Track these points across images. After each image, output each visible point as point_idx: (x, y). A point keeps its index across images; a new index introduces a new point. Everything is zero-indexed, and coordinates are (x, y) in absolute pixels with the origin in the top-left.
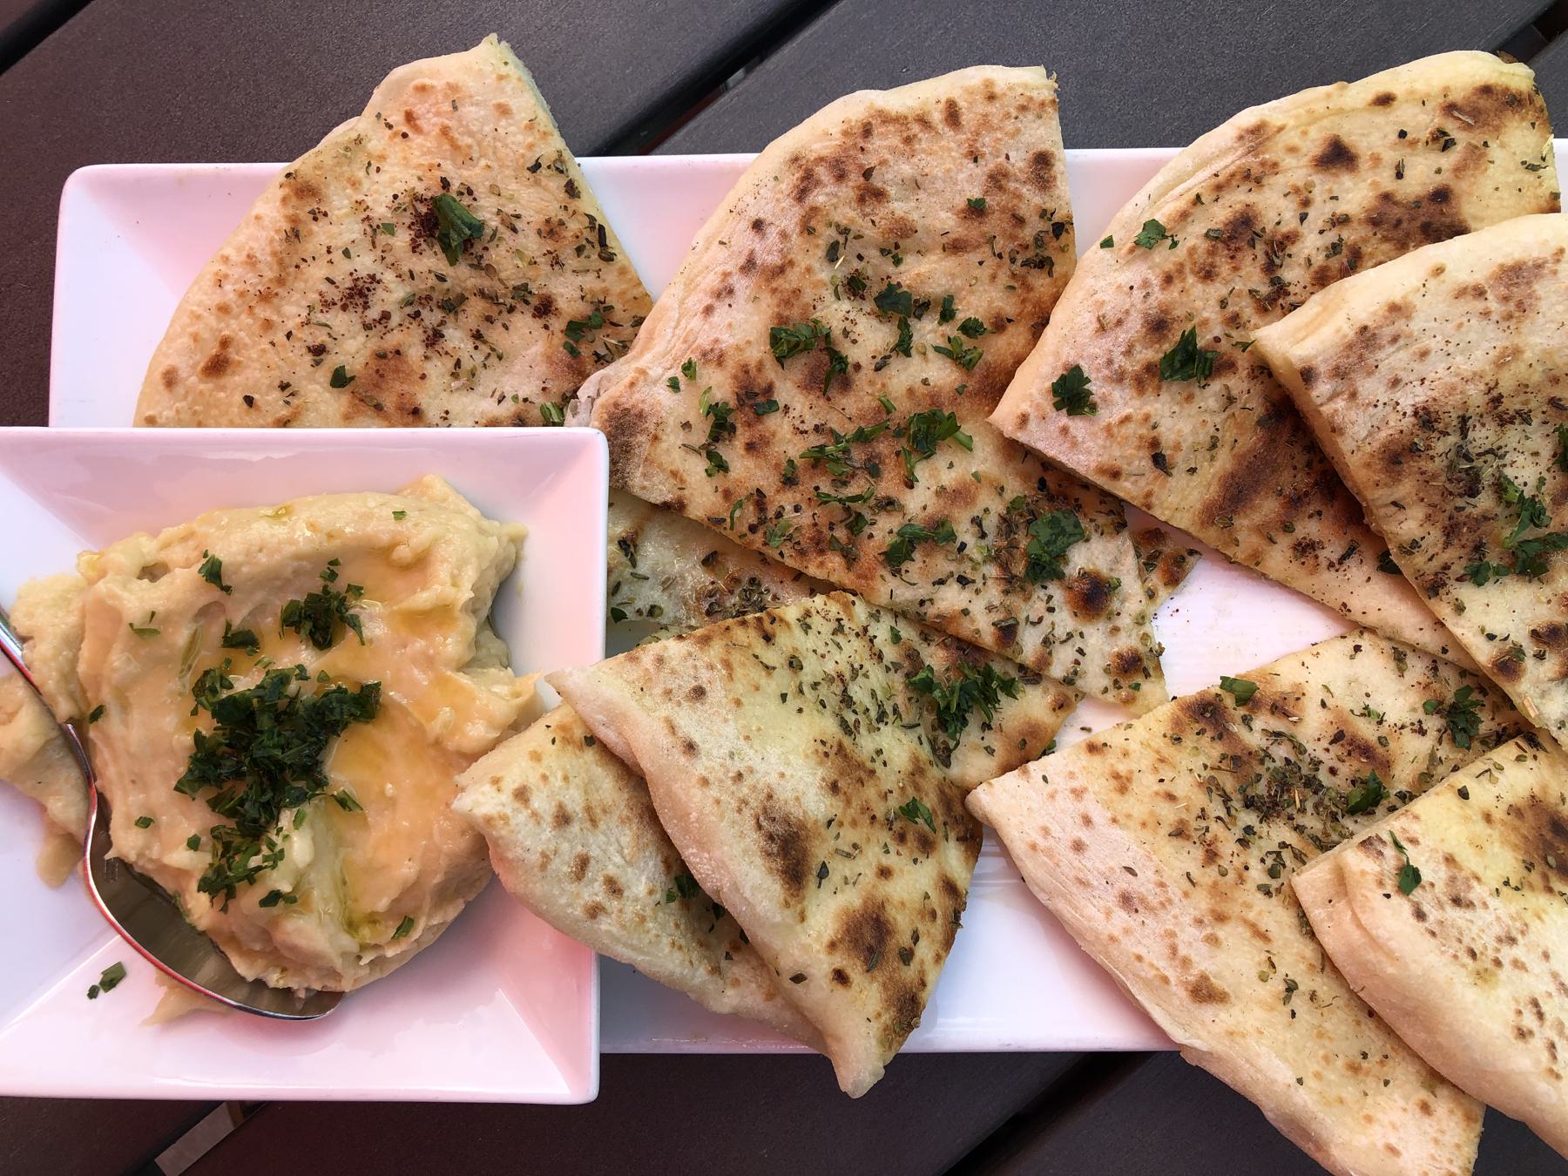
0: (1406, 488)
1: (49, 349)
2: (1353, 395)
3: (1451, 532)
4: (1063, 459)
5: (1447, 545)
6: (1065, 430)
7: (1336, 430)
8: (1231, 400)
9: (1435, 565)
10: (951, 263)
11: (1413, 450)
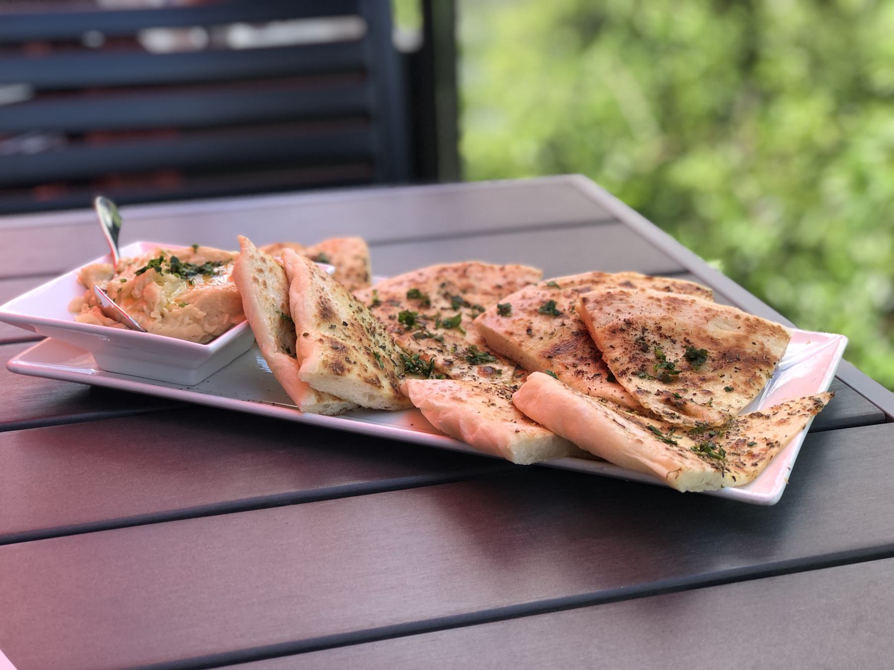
0: (617, 342)
1: (9, 655)
2: (601, 309)
3: (632, 359)
4: (494, 329)
5: (630, 362)
6: (498, 320)
7: (593, 319)
8: (563, 325)
9: (624, 368)
10: (484, 297)
11: (622, 330)
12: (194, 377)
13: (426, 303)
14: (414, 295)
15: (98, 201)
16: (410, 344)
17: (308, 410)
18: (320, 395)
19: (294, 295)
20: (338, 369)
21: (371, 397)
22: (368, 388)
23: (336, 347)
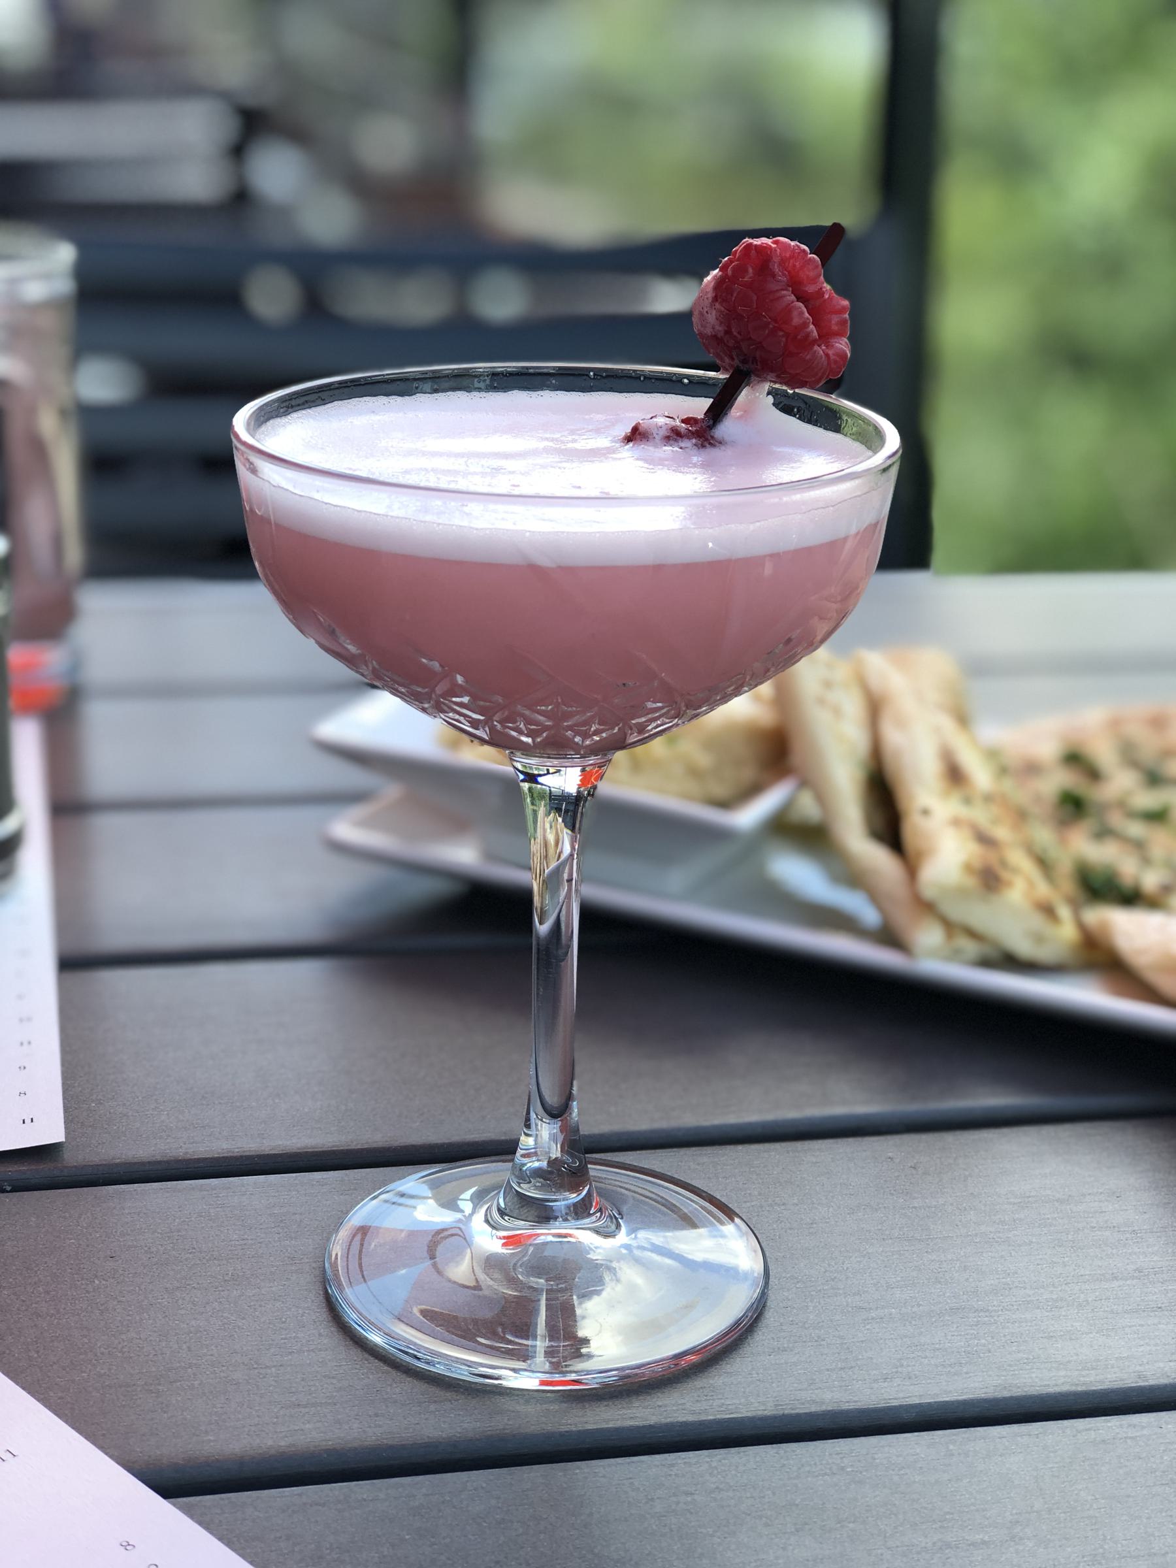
12: (678, 877)
13: (1093, 773)
14: (1075, 759)
15: (775, 449)
16: (1084, 846)
17: (933, 958)
18: (951, 927)
19: (893, 737)
20: (989, 879)
21: (1039, 939)
22: (1037, 921)
23: (984, 839)
